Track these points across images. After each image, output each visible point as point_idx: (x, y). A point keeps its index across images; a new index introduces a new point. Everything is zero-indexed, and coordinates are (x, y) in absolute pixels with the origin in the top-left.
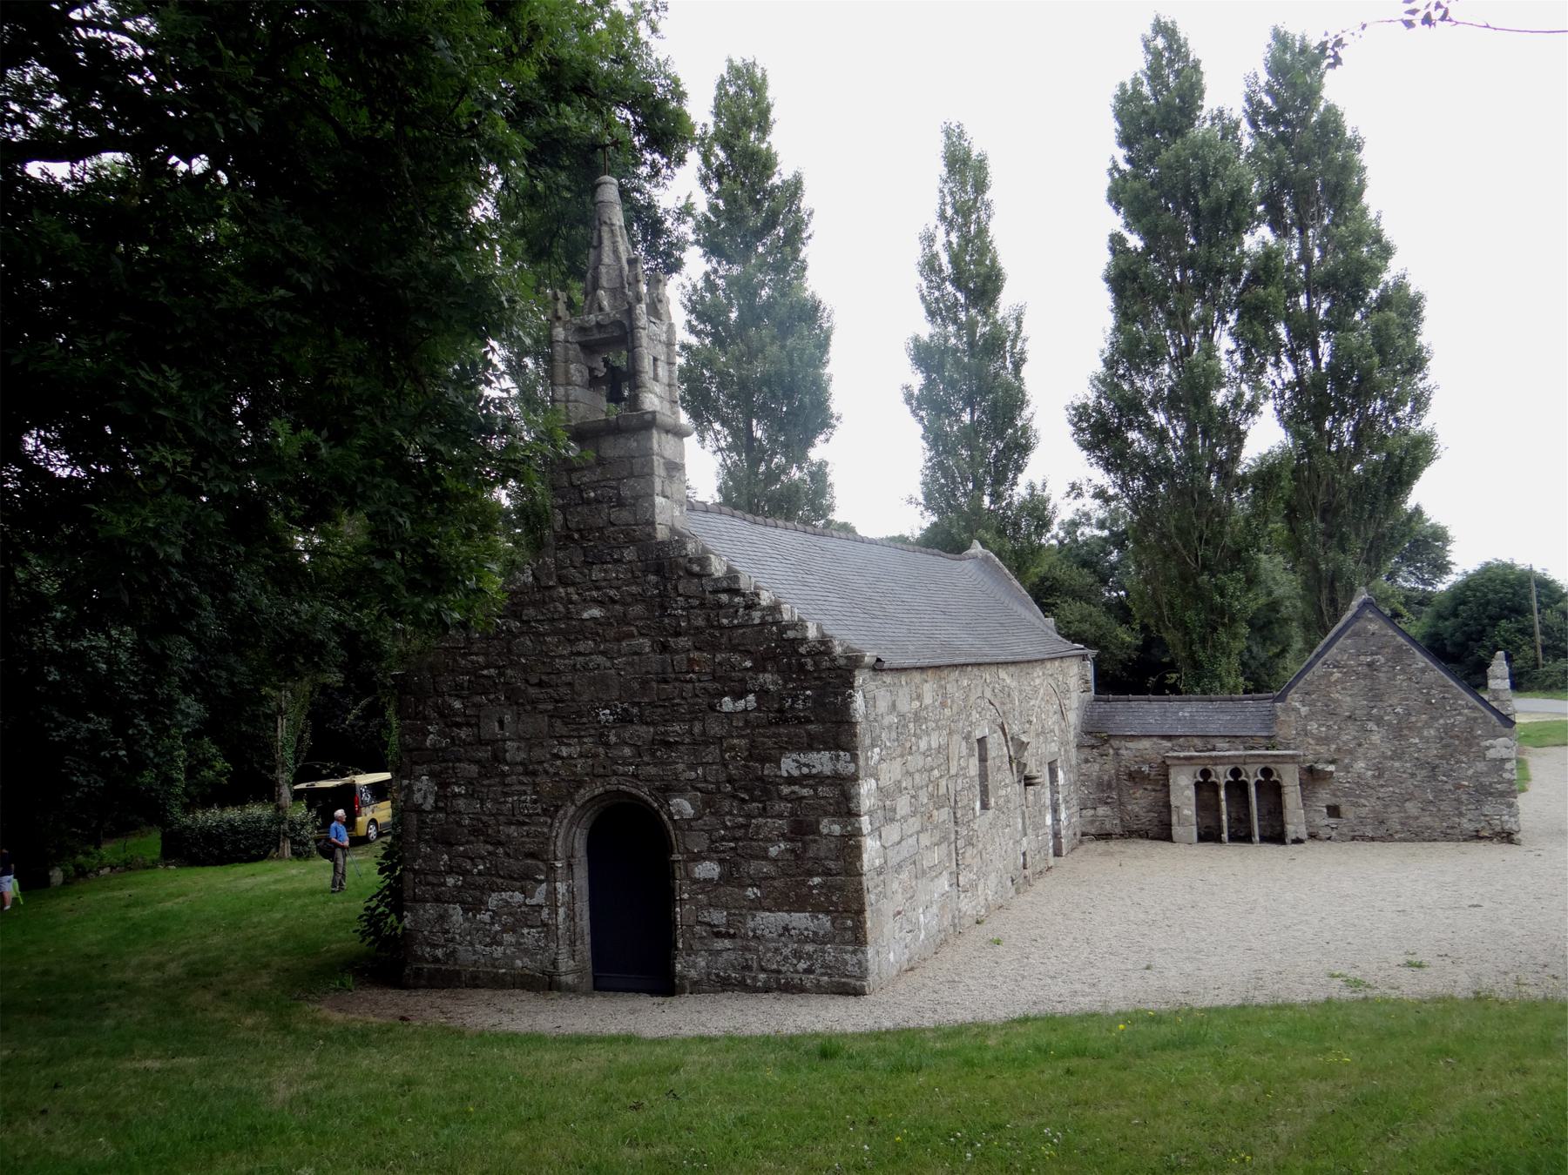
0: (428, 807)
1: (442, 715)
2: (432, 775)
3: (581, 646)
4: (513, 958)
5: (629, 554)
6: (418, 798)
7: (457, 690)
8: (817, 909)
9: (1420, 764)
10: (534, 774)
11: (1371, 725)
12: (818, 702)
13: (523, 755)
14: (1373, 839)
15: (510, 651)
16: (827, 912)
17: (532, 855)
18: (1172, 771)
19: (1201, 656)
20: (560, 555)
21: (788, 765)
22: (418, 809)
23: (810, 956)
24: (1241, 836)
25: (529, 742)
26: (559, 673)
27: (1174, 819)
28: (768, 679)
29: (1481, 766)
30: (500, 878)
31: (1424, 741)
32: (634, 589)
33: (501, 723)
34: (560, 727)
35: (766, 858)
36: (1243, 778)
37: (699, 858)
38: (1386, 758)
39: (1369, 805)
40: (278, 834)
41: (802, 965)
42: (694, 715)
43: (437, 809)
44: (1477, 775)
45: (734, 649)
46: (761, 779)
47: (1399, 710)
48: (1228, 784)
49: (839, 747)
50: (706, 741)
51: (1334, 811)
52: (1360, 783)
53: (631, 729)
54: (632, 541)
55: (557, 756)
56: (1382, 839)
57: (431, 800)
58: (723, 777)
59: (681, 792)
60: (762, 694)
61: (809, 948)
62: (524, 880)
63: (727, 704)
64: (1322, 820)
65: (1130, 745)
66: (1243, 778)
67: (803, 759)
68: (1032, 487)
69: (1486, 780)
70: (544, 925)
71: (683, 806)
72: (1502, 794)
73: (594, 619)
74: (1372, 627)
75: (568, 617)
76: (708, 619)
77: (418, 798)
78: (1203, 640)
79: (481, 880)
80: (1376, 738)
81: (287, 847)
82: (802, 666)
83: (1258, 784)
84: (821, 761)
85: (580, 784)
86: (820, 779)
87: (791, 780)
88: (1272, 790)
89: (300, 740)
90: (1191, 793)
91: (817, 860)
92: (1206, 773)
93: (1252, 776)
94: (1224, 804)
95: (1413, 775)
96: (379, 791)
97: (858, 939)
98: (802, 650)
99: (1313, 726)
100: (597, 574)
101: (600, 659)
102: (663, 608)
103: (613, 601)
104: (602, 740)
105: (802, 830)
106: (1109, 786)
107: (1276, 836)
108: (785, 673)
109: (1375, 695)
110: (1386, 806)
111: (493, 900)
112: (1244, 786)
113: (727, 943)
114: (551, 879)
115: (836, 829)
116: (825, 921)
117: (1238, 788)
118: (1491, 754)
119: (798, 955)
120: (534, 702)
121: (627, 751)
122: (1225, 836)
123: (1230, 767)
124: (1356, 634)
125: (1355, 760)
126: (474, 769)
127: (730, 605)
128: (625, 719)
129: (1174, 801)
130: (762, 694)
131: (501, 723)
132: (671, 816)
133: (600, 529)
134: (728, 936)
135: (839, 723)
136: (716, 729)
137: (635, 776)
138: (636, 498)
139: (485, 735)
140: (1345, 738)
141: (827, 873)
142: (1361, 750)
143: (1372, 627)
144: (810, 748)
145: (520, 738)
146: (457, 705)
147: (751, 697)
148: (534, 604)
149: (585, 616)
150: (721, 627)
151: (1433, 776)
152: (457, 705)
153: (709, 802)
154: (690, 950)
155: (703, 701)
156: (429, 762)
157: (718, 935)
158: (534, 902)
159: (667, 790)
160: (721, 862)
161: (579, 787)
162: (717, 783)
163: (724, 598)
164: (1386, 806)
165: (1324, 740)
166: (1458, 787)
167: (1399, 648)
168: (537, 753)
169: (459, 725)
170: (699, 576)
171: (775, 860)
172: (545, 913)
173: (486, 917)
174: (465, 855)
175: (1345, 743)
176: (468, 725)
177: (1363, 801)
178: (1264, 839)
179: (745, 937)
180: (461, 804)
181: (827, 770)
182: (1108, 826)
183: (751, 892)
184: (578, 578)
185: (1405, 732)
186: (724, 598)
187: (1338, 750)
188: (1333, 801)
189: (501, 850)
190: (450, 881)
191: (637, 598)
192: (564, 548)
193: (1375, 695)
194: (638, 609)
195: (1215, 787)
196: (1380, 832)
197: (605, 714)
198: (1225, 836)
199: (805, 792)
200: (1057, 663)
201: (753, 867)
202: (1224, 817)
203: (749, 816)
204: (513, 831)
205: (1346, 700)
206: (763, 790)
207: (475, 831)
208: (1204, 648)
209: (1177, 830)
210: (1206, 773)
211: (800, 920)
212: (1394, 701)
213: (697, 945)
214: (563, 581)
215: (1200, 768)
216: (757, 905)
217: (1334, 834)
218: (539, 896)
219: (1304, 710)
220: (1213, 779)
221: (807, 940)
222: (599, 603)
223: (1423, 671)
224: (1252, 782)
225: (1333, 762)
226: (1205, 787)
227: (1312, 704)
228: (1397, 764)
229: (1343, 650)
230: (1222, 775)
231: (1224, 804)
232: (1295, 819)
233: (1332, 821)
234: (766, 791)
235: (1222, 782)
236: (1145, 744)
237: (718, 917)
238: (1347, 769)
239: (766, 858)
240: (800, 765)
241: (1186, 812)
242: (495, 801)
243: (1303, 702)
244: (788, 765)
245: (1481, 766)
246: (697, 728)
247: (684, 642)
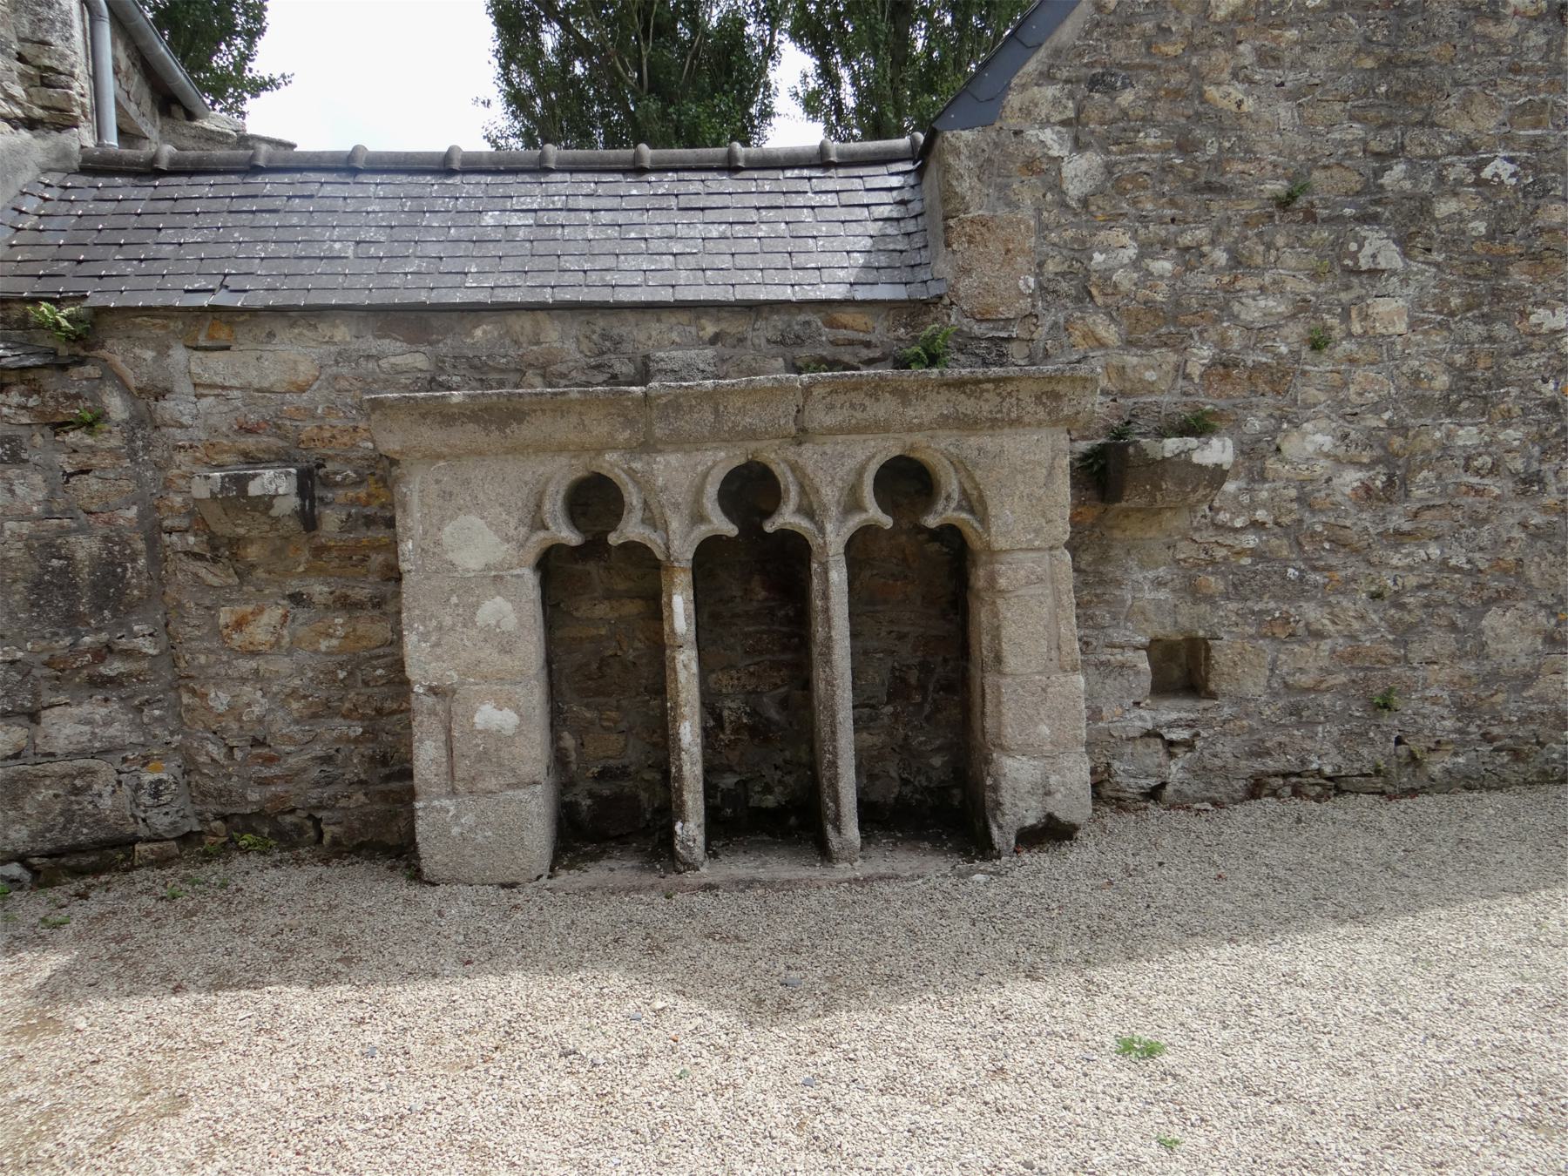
11: (1377, 246)
14: (1336, 786)
18: (417, 492)
24: (773, 812)
27: (427, 755)
36: (787, 518)
38: (1422, 403)
39: (1340, 620)
47: (1500, 168)
48: (709, 553)
51: (1183, 669)
65: (216, 367)
66: (787, 518)
80: (1390, 311)
83: (860, 548)
88: (932, 576)
90: (513, 613)
92: (594, 499)
93: (830, 507)
94: (685, 664)
95: (1529, 482)
99: (1115, 253)
106: (109, 588)
107: (942, 808)
110: (1404, 634)
112: (787, 562)
117: (759, 569)
122: (690, 829)
123: (721, 460)
125: (1289, 418)
129: (423, 661)
140: (1255, 309)
142: (1318, 368)
164: (1404, 634)
165: (1160, 324)
175: (1258, 334)
177: (1312, 612)
182: (108, 801)
185: (1519, 276)
187: (1224, 366)
195: (646, 567)
198: (690, 829)
200: (266, 384)
202: (688, 732)
209: (441, 819)
210: (594, 499)
212: (1485, 122)
215: (561, 473)
217: (1175, 771)
220: (631, 529)
224: (833, 539)
226: (588, 568)
227: (1120, 134)
228: (1468, 436)
230: (676, 504)
231: (685, 664)
232: (1045, 715)
233: (1171, 712)
235: (682, 545)
241: (491, 716)
243: (1078, 134)
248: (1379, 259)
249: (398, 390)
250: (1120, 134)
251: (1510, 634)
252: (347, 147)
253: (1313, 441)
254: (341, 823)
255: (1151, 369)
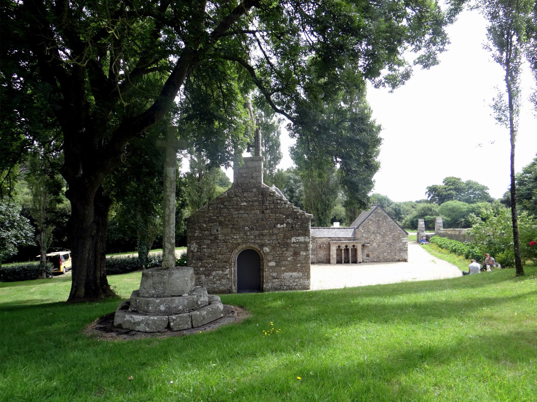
0: (195, 251)
1: (200, 228)
2: (196, 243)
3: (241, 212)
4: (220, 287)
5: (254, 190)
6: (192, 249)
7: (205, 222)
8: (299, 271)
9: (388, 244)
10: (226, 242)
11: (378, 235)
12: (301, 225)
13: (223, 238)
15: (220, 212)
16: (301, 272)
17: (225, 262)
18: (331, 246)
19: (322, 218)
20: (235, 189)
21: (293, 240)
22: (192, 252)
23: (297, 282)
24: (347, 262)
25: (225, 235)
26: (234, 218)
28: (290, 220)
29: (401, 244)
30: (215, 268)
31: (389, 239)
32: (256, 199)
33: (217, 231)
34: (234, 231)
35: (287, 260)
37: (270, 261)
39: (376, 253)
40: (42, 270)
41: (295, 284)
42: (270, 228)
43: (198, 251)
44: (400, 246)
45: (281, 213)
46: (287, 243)
49: (305, 236)
50: (273, 234)
51: (368, 256)
52: (374, 249)
53: (253, 231)
54: (255, 187)
55: (233, 238)
56: (378, 262)
57: (196, 249)
58: (277, 242)
59: (266, 246)
60: (288, 223)
61: (297, 280)
62: (223, 268)
63: (279, 226)
64: (365, 258)
67: (297, 238)
68: (278, 170)
69: (402, 247)
70: (228, 278)
71: (267, 249)
72: (405, 251)
73: (244, 205)
74: (379, 211)
75: (237, 205)
76: (275, 206)
77: (192, 249)
78: (322, 214)
79: (210, 269)
80: (378, 238)
81: (45, 275)
82: (297, 218)
84: (302, 239)
85: (239, 244)
86: (300, 243)
87: (294, 243)
88: (355, 250)
89: (49, 239)
90: (335, 251)
91: (299, 261)
92: (339, 246)
93: (350, 247)
96: (66, 257)
97: (308, 277)
98: (298, 214)
99: (364, 235)
100: (245, 194)
101: (246, 215)
102: (263, 203)
103: (250, 201)
104: (245, 234)
105: (296, 254)
107: (355, 262)
108: (293, 219)
109: (379, 227)
111: (214, 273)
113: (277, 280)
114: (230, 268)
115: (304, 254)
116: (301, 274)
117: (347, 250)
118: (403, 241)
119: (294, 282)
120: (227, 225)
121: (252, 237)
124: (376, 213)
126: (209, 241)
127: (280, 203)
128: (252, 229)
130: (288, 223)
131: (217, 231)
132: (263, 252)
133: (247, 184)
134: (277, 278)
135: (306, 230)
136: (275, 231)
137: (254, 243)
138: (257, 177)
139: (213, 233)
141: (302, 263)
143: (379, 211)
144: (299, 236)
145: (223, 234)
146: (205, 226)
147: (285, 224)
148: (228, 201)
149: (242, 204)
150: (278, 208)
151: (390, 247)
152: (205, 226)
153: (273, 248)
154: (267, 282)
155: (272, 225)
156: (196, 240)
157: (274, 278)
158: (226, 273)
159: (262, 246)
160: (276, 262)
161: (239, 245)
162: (276, 244)
163: (279, 201)
165: (367, 238)
166: (396, 249)
167: (385, 216)
168: (227, 237)
169: (205, 231)
170: (273, 196)
171: (289, 261)
172: (228, 276)
173: (212, 277)
174: (206, 263)
176: (208, 230)
178: (352, 263)
179: (281, 278)
180: (205, 250)
181: (303, 241)
183: (283, 268)
184: (240, 195)
186: (279, 201)
188: (368, 253)
189: (216, 261)
190: (201, 269)
191: (256, 201)
192: (237, 188)
193: (379, 227)
194: (256, 203)
196: (378, 261)
197: (246, 228)
199: (297, 246)
201: (284, 263)
203: (283, 251)
204: (220, 256)
205: (372, 228)
206: (287, 245)
207: (209, 257)
208: (323, 215)
209: (332, 261)
210: (339, 246)
211: (295, 274)
213: (269, 281)
214: (236, 196)
216: (285, 271)
218: (227, 271)
219: (363, 231)
221: (296, 278)
222: (246, 202)
223: (390, 222)
225: (368, 244)
226: (339, 249)
229: (372, 216)
230: (343, 247)
232: (360, 258)
234: (288, 246)
236: (324, 239)
237: (275, 274)
238: (371, 245)
239: (287, 260)
240: (296, 240)
242: (215, 249)
244: (293, 240)
245: (401, 244)
246: (271, 232)
247: (268, 211)
248: (163, 263)
249: (285, 295)
250: (365, 229)
251: (385, 254)
252: (342, 287)
253: (375, 244)
254: (328, 261)
255: (366, 240)
